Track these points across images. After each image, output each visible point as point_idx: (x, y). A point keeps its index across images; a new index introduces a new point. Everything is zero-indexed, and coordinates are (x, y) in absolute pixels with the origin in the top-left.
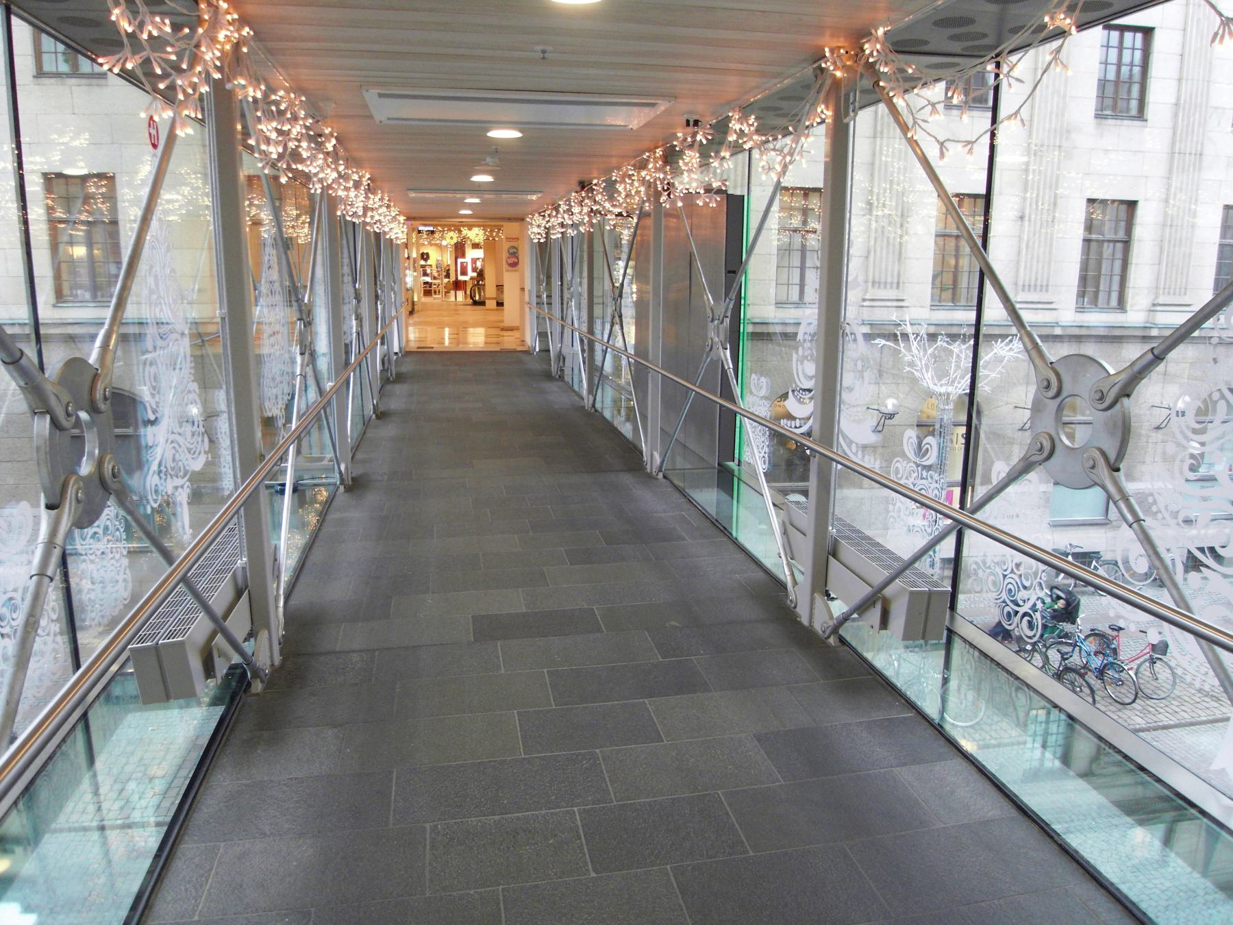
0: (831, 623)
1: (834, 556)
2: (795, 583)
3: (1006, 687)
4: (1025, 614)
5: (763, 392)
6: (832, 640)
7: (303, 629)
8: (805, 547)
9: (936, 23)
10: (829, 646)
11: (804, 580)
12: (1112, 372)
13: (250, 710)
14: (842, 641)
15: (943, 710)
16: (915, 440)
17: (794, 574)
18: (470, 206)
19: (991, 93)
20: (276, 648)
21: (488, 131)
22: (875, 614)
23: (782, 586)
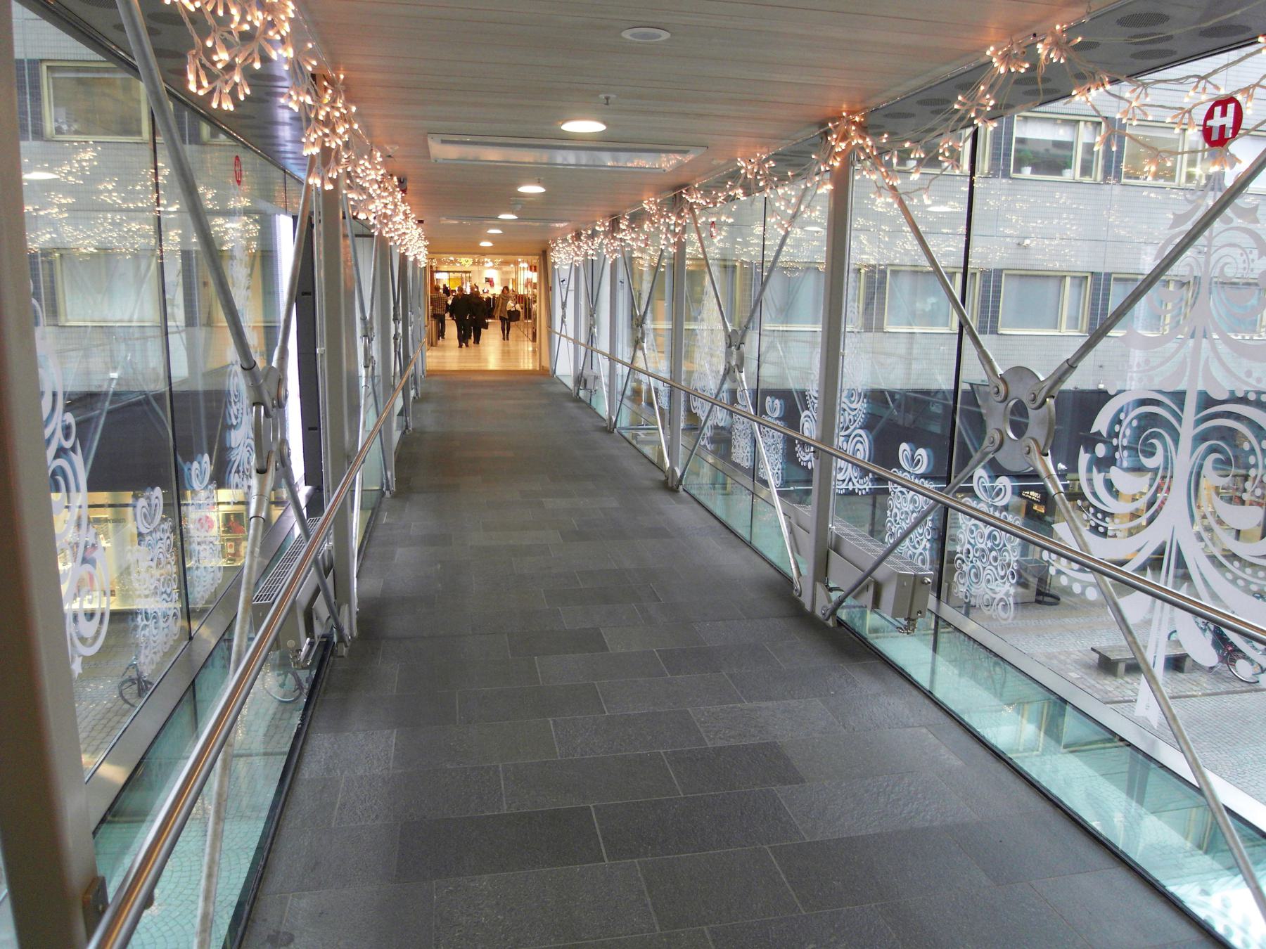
0: (830, 606)
1: (837, 550)
2: (799, 574)
3: (986, 665)
4: (1001, 600)
5: (777, 414)
6: (830, 623)
7: (373, 618)
8: (808, 542)
9: (1121, 22)
10: (827, 627)
11: (807, 569)
12: (1042, 379)
13: (331, 674)
14: (840, 623)
15: (932, 682)
16: (909, 452)
17: (798, 566)
18: (491, 238)
19: (969, 144)
20: (354, 617)
21: (520, 185)
22: (868, 597)
23: (789, 581)
